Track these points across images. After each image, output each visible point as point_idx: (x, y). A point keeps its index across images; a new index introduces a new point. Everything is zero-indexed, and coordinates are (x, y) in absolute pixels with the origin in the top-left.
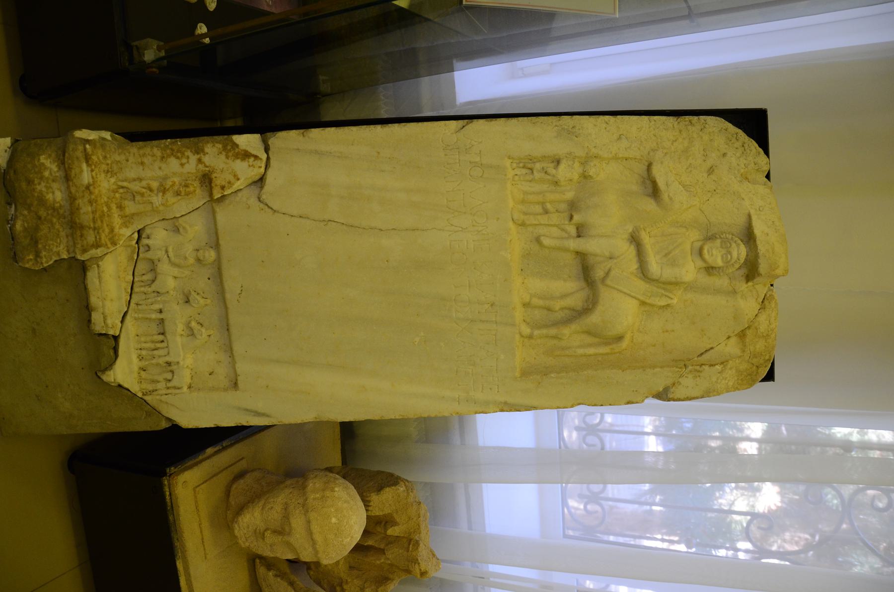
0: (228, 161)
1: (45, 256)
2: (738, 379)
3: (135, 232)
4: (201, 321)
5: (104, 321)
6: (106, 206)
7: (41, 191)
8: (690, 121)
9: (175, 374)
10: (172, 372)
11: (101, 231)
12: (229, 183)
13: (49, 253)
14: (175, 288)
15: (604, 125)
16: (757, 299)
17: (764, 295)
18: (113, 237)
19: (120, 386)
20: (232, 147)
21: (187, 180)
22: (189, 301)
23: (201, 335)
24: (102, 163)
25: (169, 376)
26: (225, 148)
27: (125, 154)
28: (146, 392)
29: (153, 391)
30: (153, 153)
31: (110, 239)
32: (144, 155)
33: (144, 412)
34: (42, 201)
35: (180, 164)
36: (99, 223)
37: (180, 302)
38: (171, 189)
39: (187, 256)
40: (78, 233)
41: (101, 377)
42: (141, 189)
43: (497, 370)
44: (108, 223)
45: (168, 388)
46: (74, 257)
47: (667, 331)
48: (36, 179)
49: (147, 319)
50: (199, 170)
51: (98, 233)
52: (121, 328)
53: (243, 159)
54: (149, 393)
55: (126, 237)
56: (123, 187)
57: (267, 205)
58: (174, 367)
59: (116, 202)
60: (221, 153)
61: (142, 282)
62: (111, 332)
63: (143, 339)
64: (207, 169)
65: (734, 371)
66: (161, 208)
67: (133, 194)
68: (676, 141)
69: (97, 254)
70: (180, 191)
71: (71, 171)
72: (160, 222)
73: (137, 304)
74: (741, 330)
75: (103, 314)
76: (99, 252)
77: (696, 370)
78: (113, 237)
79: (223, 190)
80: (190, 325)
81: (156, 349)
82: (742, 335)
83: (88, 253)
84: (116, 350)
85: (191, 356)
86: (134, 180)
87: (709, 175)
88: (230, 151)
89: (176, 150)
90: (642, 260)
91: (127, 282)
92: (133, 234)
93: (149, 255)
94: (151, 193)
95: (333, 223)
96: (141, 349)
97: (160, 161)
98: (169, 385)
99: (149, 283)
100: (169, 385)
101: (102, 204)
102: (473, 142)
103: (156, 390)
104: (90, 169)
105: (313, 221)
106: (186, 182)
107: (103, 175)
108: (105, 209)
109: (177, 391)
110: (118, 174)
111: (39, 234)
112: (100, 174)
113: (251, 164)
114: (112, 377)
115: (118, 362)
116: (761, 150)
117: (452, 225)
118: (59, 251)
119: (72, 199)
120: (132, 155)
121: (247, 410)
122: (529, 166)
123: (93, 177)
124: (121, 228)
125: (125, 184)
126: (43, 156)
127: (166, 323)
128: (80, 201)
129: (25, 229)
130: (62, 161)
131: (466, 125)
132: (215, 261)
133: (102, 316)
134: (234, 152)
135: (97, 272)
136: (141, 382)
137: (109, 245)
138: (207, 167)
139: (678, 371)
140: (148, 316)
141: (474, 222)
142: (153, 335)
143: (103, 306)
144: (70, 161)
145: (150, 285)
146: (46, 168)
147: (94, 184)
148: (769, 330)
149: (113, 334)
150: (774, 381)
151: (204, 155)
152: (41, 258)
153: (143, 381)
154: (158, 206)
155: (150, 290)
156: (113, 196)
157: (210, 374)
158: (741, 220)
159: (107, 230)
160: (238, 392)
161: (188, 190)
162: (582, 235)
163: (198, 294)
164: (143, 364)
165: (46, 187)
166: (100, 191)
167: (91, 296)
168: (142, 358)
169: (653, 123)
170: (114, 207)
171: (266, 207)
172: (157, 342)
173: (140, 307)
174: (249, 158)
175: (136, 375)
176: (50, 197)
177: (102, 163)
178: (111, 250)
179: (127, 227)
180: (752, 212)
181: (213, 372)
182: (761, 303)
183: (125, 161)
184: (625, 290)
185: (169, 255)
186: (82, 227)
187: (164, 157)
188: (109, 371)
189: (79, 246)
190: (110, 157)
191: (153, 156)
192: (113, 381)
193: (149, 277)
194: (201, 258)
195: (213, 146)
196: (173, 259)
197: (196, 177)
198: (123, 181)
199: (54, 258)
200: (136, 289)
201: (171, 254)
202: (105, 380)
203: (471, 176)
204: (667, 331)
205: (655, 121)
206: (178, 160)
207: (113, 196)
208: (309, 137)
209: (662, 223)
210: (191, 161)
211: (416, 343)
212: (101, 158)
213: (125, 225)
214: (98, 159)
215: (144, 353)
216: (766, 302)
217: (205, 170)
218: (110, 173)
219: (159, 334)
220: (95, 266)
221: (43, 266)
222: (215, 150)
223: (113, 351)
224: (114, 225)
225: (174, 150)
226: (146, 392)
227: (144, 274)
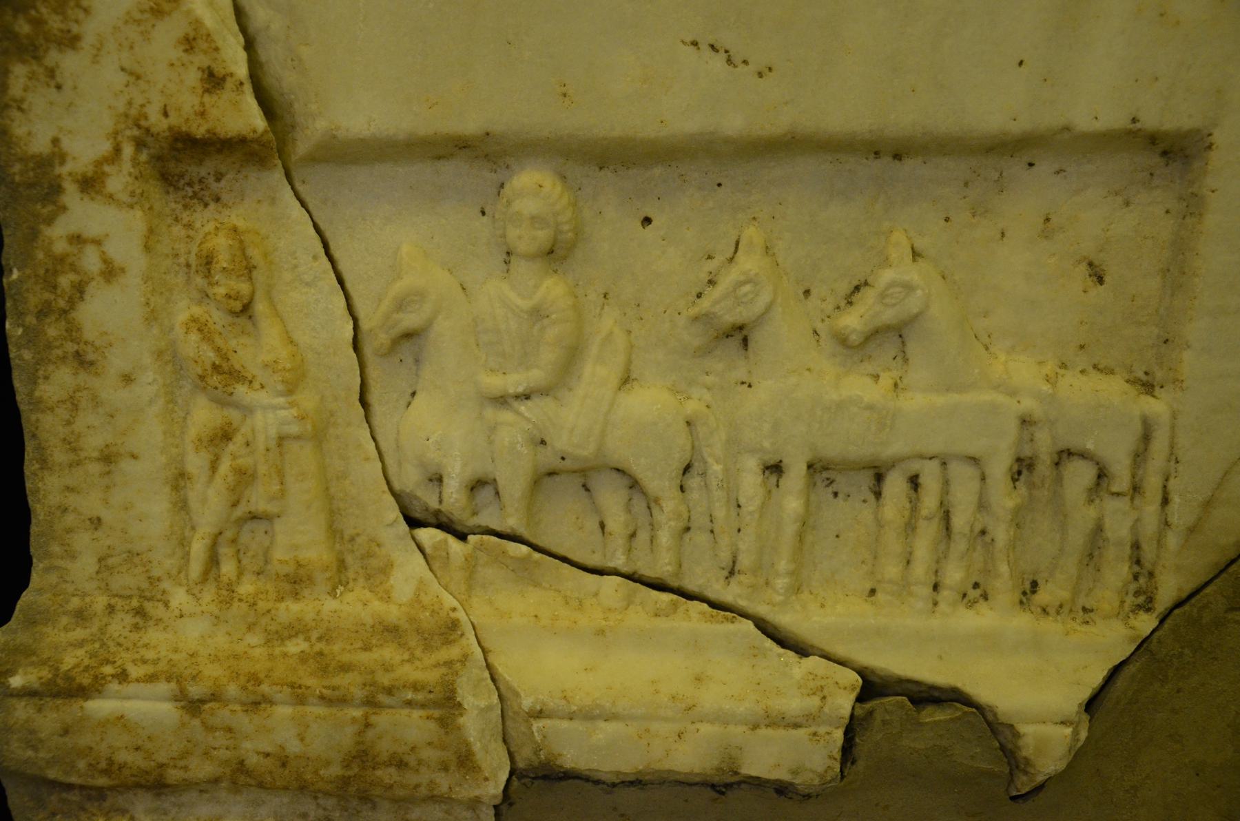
0: (88, 40)
3: (414, 538)
4: (844, 287)
5: (787, 726)
9: (1074, 442)
10: (1065, 455)
11: (385, 680)
14: (674, 390)
18: (418, 631)
19: (1091, 705)
21: (188, 266)
22: (741, 328)
23: (909, 288)
24: (102, 630)
25: (1080, 475)
27: (69, 531)
28: (1137, 593)
29: (1138, 562)
31: (428, 648)
32: (72, 445)
33: (1230, 616)
35: (108, 281)
36: (350, 683)
37: (741, 373)
38: (219, 342)
39: (525, 304)
40: (387, 775)
41: (1040, 779)
42: (218, 480)
44: (359, 644)
45: (1136, 489)
46: (496, 807)
49: (800, 537)
50: (132, 194)
51: (389, 691)
52: (827, 657)
54: (1142, 580)
55: (430, 574)
56: (213, 560)
59: (272, 595)
60: (51, 73)
61: (633, 535)
62: (844, 703)
63: (892, 570)
66: (307, 400)
67: (241, 522)
69: (489, 708)
70: (228, 296)
71: (122, 767)
72: (377, 420)
73: (732, 573)
75: (755, 727)
78: (418, 631)
79: (223, 79)
80: (854, 338)
81: (947, 517)
83: (477, 747)
85: (1002, 357)
86: (182, 506)
88: (38, 23)
89: (47, 296)
91: (629, 601)
92: (421, 549)
93: (514, 483)
94: (239, 439)
96: (936, 587)
99: (644, 505)
100: (1122, 482)
101: (271, 657)
103: (1136, 546)
104: (114, 686)
106: (194, 268)
107: (153, 635)
108: (295, 647)
109: (1159, 445)
110: (156, 573)
112: (146, 646)
115: (982, 692)
120: (72, 500)
123: (151, 678)
124: (387, 592)
125: (198, 548)
127: (832, 449)
130: (89, 798)
132: (563, 178)
133: (763, 732)
135: (565, 724)
136: (1085, 610)
137: (454, 652)
138: (117, 150)
140: (790, 529)
142: (880, 524)
143: (722, 718)
144: (82, 765)
145: (652, 503)
147: (179, 679)
149: (853, 696)
151: (62, 158)
153: (1082, 601)
154: (294, 412)
155: (670, 503)
156: (244, 606)
157: (1101, 280)
159: (389, 653)
160: (1218, 137)
161: (223, 260)
163: (711, 282)
164: (1004, 585)
166: (215, 659)
167: (666, 765)
168: (976, 585)
170: (290, 610)
172: (914, 509)
173: (745, 561)
175: (1051, 627)
177: (102, 630)
178: (478, 651)
179: (387, 569)
181: (1090, 264)
183: (98, 534)
185: (520, 390)
186: (362, 756)
187: (78, 354)
188: (1021, 743)
189: (444, 783)
190: (84, 595)
192: (1068, 731)
193: (612, 499)
194: (543, 236)
195: (20, 109)
196: (536, 376)
197: (177, 219)
198: (186, 556)
200: (662, 568)
201: (514, 382)
202: (1061, 766)
206: (91, 289)
207: (244, 606)
210: (93, 229)
212: (79, 634)
214: (81, 644)
215: (954, 575)
217: (135, 162)
218: (148, 606)
219: (878, 494)
220: (537, 725)
222: (39, 100)
223: (930, 709)
225: (48, 303)
227: (602, 526)
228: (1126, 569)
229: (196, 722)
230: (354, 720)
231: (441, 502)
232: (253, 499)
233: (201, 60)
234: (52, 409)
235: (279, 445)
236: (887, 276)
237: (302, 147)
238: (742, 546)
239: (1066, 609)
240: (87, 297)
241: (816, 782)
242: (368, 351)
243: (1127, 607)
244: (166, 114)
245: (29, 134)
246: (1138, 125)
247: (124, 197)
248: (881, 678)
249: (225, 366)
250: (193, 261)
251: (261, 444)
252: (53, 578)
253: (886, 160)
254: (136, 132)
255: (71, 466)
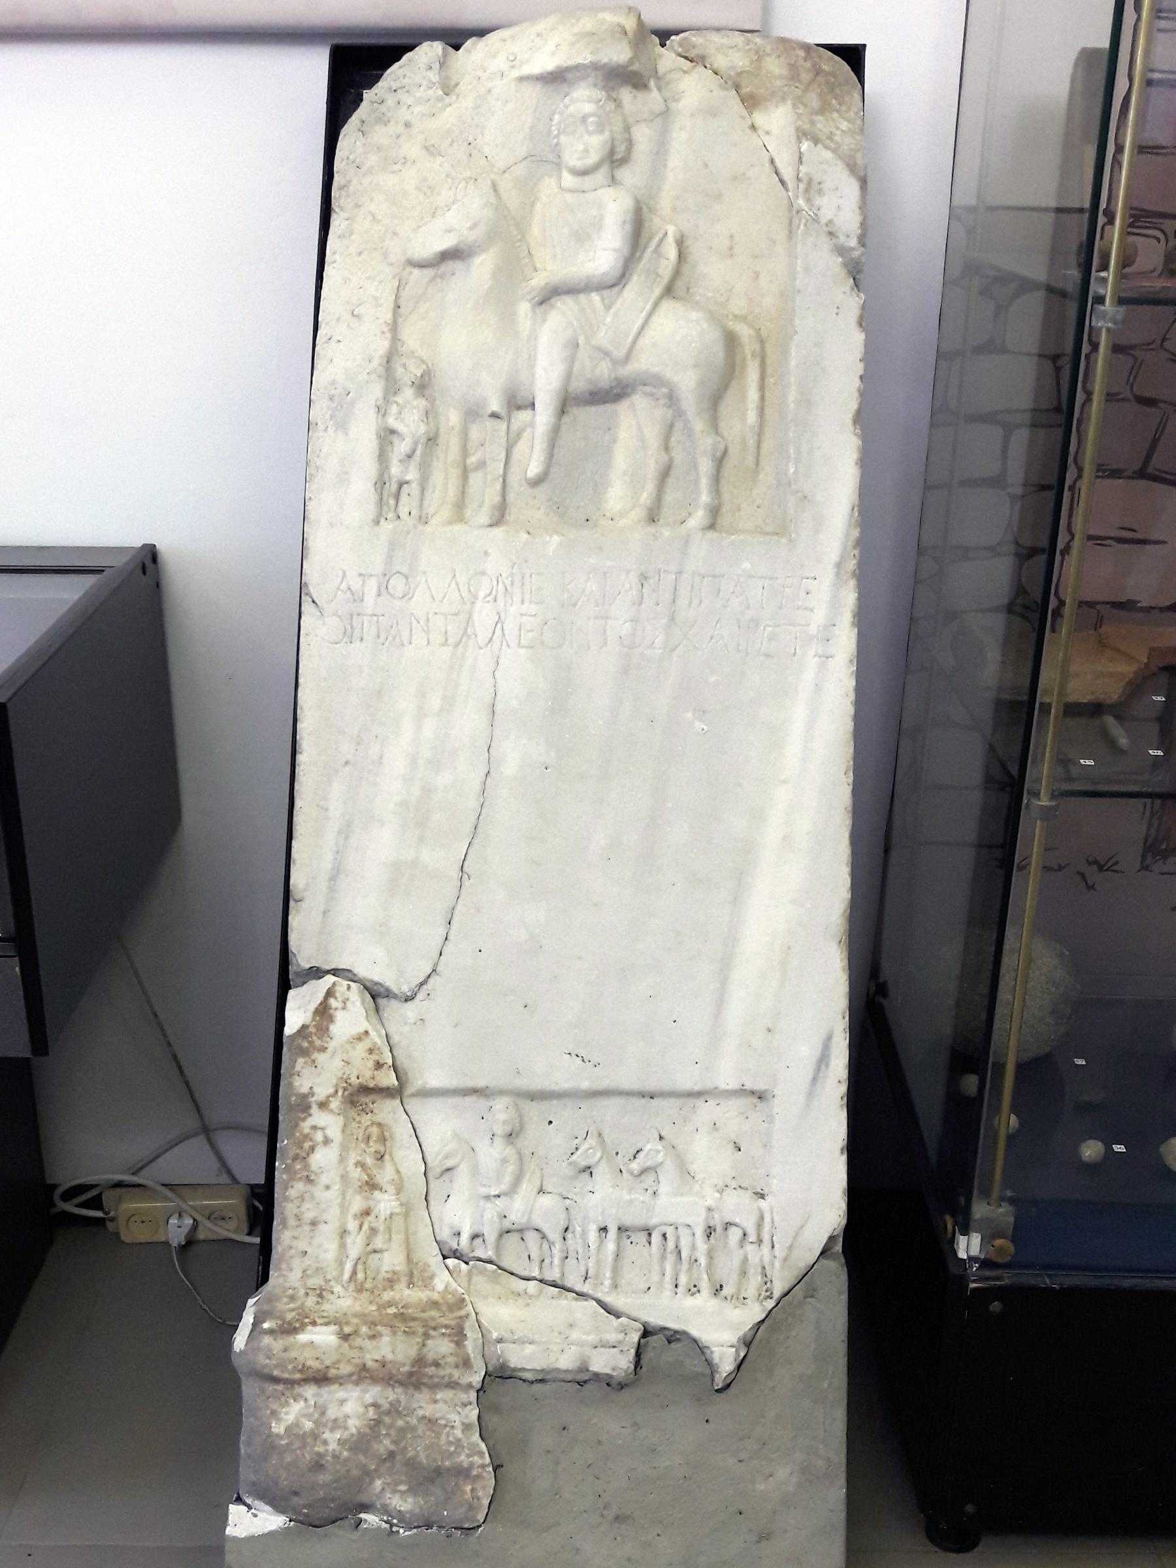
1: (469, 1456)
2: (838, 111)
6: (385, 1308)
7: (340, 1442)
8: (341, 188)
10: (728, 1225)
12: (371, 1051)
13: (463, 1447)
15: (333, 343)
16: (685, 72)
17: (679, 58)
20: (305, 1038)
25: (735, 1234)
26: (305, 1053)
28: (766, 1291)
30: (297, 1198)
32: (298, 1217)
34: (360, 1444)
40: (431, 1370)
43: (771, 579)
47: (731, 248)
48: (316, 1449)
53: (331, 1019)
54: (768, 1284)
56: (354, 1273)
57: (422, 984)
58: (717, 1221)
60: (314, 1061)
62: (635, 1337)
64: (340, 1093)
65: (820, 118)
67: (370, 1253)
68: (373, 216)
72: (431, 1209)
74: (741, 105)
76: (472, 1334)
77: (807, 191)
82: (751, 102)
84: (673, 1337)
86: (343, 1246)
87: (440, 154)
88: (311, 1043)
90: (587, 285)
91: (540, 1292)
93: (491, 1236)
94: (373, 1215)
95: (466, 863)
96: (676, 1286)
97: (315, 1185)
98: (752, 1237)
100: (752, 1237)
102: (341, 587)
105: (460, 900)
110: (329, 1277)
111: (424, 1461)
113: (340, 1005)
114: (725, 1349)
116: (405, 58)
117: (491, 640)
118: (463, 1424)
119: (363, 1375)
120: (295, 1243)
121: (815, 1080)
122: (394, 487)
123: (326, 1324)
125: (348, 1267)
126: (273, 1425)
127: (628, 1221)
128: (368, 1356)
129: (412, 1491)
131: (311, 597)
134: (315, 1034)
135: (512, 1346)
137: (463, 1313)
138: (336, 1092)
139: (805, 225)
140: (610, 1258)
141: (489, 599)
146: (297, 1424)
148: (748, 47)
150: (865, 46)
152: (471, 1465)
157: (740, 1150)
158: (532, 92)
162: (531, 399)
165: (332, 1430)
169: (337, 257)
171: (425, 987)
174: (330, 1009)
175: (726, 1304)
176: (354, 1424)
178: (474, 1314)
179: (432, 1277)
180: (516, 73)
182: (693, 64)
184: (639, 323)
189: (456, 1374)
191: (302, 1198)
192: (734, 1350)
196: (504, 1187)
198: (342, 1270)
199: (476, 1437)
200: (553, 1274)
203: (403, 597)
204: (731, 248)
205: (334, 253)
206: (317, 1149)
208: (305, 890)
209: (520, 246)
210: (321, 1123)
211: (705, 728)
212: (292, 1306)
213: (427, 1281)
214: (292, 1310)
216: (692, 55)
219: (650, 1243)
221: (488, 1465)
222: (307, 1072)
224: (425, 1299)
226: (766, 1291)
227: (529, 1257)
228: (760, 1278)
229: (346, 1345)
230: (418, 1343)
231: (458, 1245)
232: (376, 1242)
233: (375, 1057)
234: (292, 1201)
235: (391, 1217)
236: (649, 1147)
237: (410, 1089)
238: (590, 1265)
239: (735, 1297)
240: (315, 1152)
241: (623, 1374)
242: (430, 1175)
243: (762, 1297)
244: (358, 1078)
245: (301, 1085)
246: (744, 1088)
247: (337, 1111)
248: (652, 1327)
249: (371, 1183)
250: (360, 1136)
251: (382, 1218)
252: (281, 1280)
253: (647, 1099)
254: (345, 1085)
255: (297, 1227)
